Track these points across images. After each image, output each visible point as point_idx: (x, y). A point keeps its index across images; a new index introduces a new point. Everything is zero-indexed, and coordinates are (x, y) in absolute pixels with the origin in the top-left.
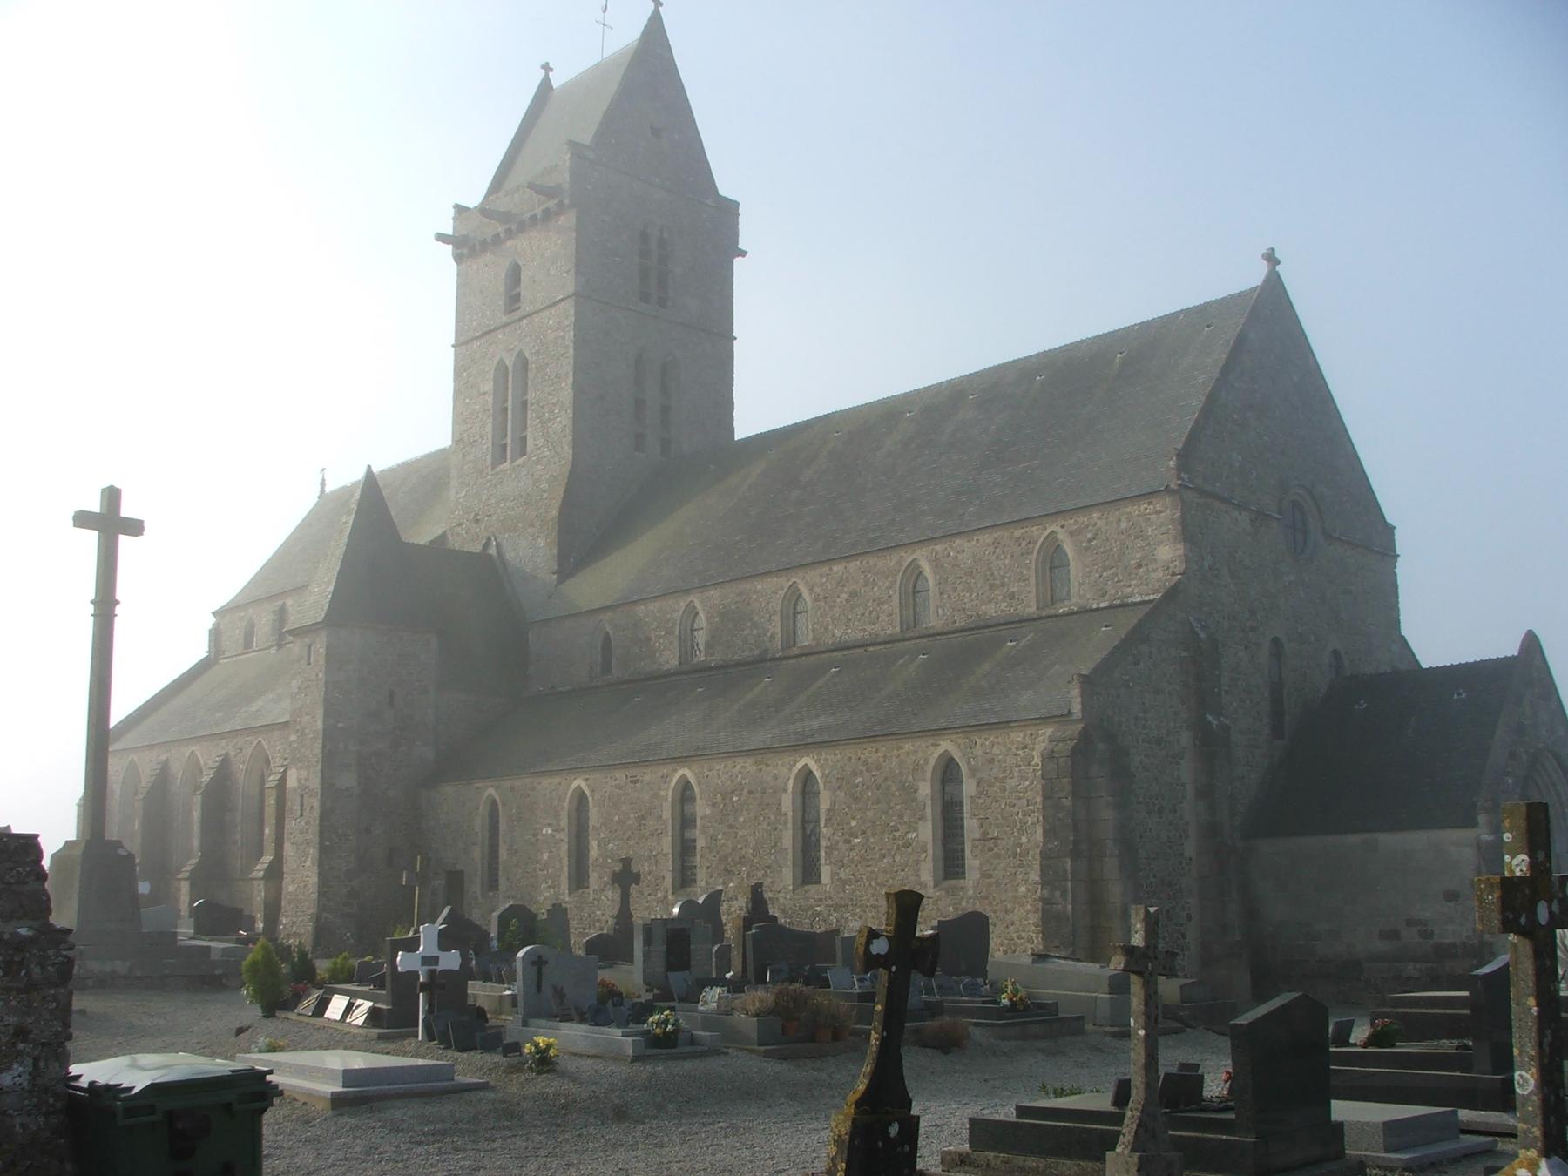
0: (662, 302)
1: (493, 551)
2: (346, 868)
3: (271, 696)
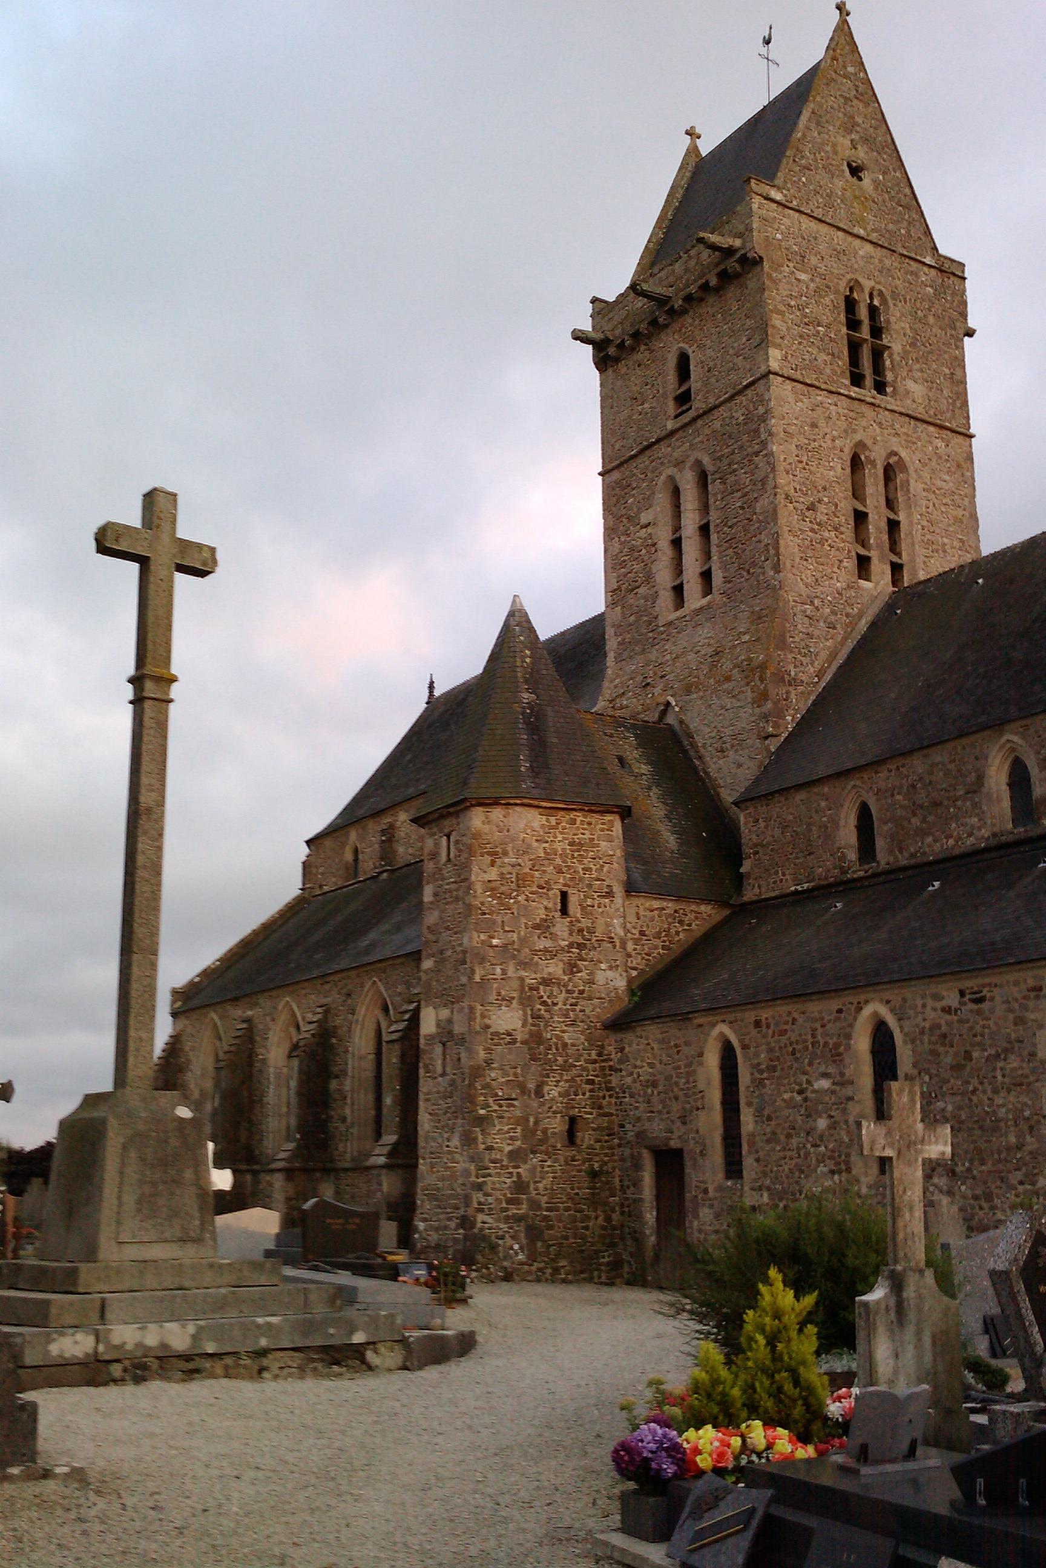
0: (880, 387)
1: (670, 719)
2: (510, 1148)
3: (386, 927)
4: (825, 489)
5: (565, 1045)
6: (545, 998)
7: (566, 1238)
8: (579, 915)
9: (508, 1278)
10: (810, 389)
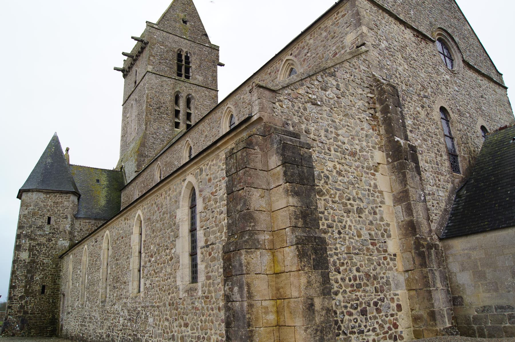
0: (188, 77)
4: (164, 103)
5: (44, 264)
6: (38, 249)
7: (36, 323)
8: (54, 224)
9: (13, 335)
10: (162, 77)
